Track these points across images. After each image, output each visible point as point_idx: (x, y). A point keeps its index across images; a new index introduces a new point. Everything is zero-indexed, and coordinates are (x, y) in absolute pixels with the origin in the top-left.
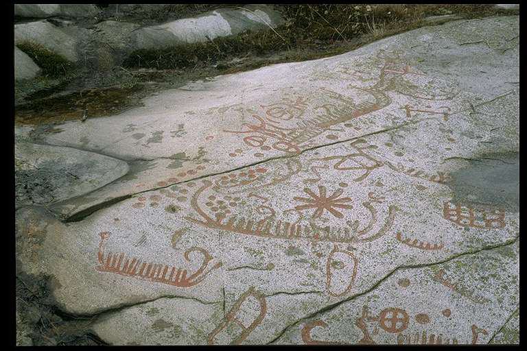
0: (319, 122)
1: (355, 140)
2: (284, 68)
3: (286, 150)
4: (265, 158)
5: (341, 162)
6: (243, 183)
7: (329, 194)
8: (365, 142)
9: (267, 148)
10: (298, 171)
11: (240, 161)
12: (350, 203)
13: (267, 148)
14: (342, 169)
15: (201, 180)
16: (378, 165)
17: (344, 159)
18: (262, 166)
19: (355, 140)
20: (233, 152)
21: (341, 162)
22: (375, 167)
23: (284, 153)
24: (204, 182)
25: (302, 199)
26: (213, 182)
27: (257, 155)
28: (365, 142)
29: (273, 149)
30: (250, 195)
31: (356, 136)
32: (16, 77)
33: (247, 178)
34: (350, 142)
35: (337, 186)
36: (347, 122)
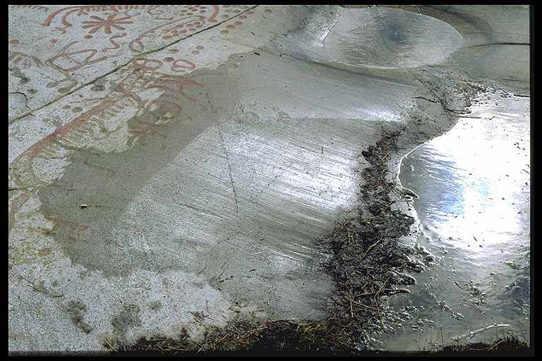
0: (114, 107)
1: (72, 89)
2: (395, 349)
3: (147, 61)
4: (166, 50)
5: (90, 57)
6: (180, 26)
7: (103, 28)
8: (60, 90)
9: (169, 59)
10: (132, 43)
11: (191, 43)
12: (83, 25)
13: (169, 59)
14: (89, 50)
15: (219, 22)
16: (51, 61)
17: (86, 62)
18: (168, 42)
19: (72, 89)
20: (200, 51)
21: (90, 57)
22: (54, 58)
23: (149, 57)
24: (216, 21)
25: (127, 22)
26: (207, 23)
27: (176, 51)
28: (60, 90)
29: (161, 59)
30: (171, 19)
31: (70, 95)
32: (526, 103)
33: (179, 30)
34: (78, 86)
35: (94, 35)
36: (79, 114)
